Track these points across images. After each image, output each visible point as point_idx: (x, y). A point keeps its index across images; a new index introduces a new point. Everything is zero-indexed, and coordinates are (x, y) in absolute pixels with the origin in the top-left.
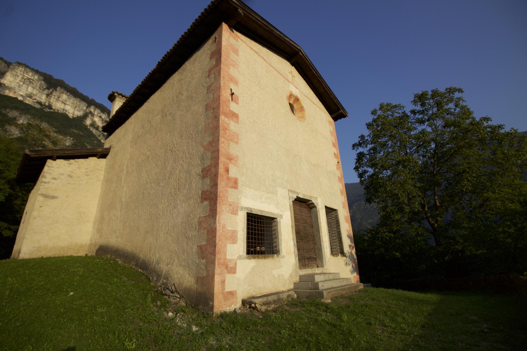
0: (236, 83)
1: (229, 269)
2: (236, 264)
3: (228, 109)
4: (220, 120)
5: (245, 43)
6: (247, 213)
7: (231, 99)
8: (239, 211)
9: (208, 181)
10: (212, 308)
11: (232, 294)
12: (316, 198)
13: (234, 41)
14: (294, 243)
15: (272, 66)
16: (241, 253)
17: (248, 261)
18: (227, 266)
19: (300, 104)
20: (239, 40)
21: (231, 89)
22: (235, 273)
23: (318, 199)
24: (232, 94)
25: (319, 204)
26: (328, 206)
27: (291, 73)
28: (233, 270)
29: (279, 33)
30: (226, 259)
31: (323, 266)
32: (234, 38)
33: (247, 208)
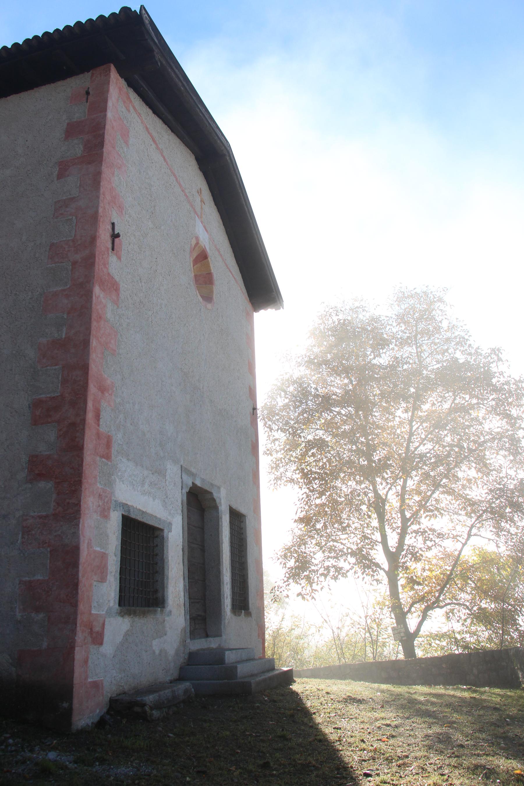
0: (121, 208)
1: (94, 635)
2: (104, 624)
3: (105, 270)
4: (94, 298)
5: (139, 115)
6: (123, 516)
7: (110, 246)
8: (111, 510)
9: (51, 434)
10: (69, 713)
11: (96, 685)
12: (219, 488)
13: (124, 109)
14: (185, 586)
15: (175, 176)
16: (112, 604)
17: (120, 619)
18: (91, 629)
19: (208, 266)
20: (131, 108)
21: (113, 224)
22: (101, 644)
23: (222, 489)
24: (115, 236)
25: (223, 501)
26: (234, 507)
27: (200, 192)
28: (98, 638)
29: (198, 110)
30: (90, 613)
31: (219, 635)
32: (124, 102)
33: (124, 505)
